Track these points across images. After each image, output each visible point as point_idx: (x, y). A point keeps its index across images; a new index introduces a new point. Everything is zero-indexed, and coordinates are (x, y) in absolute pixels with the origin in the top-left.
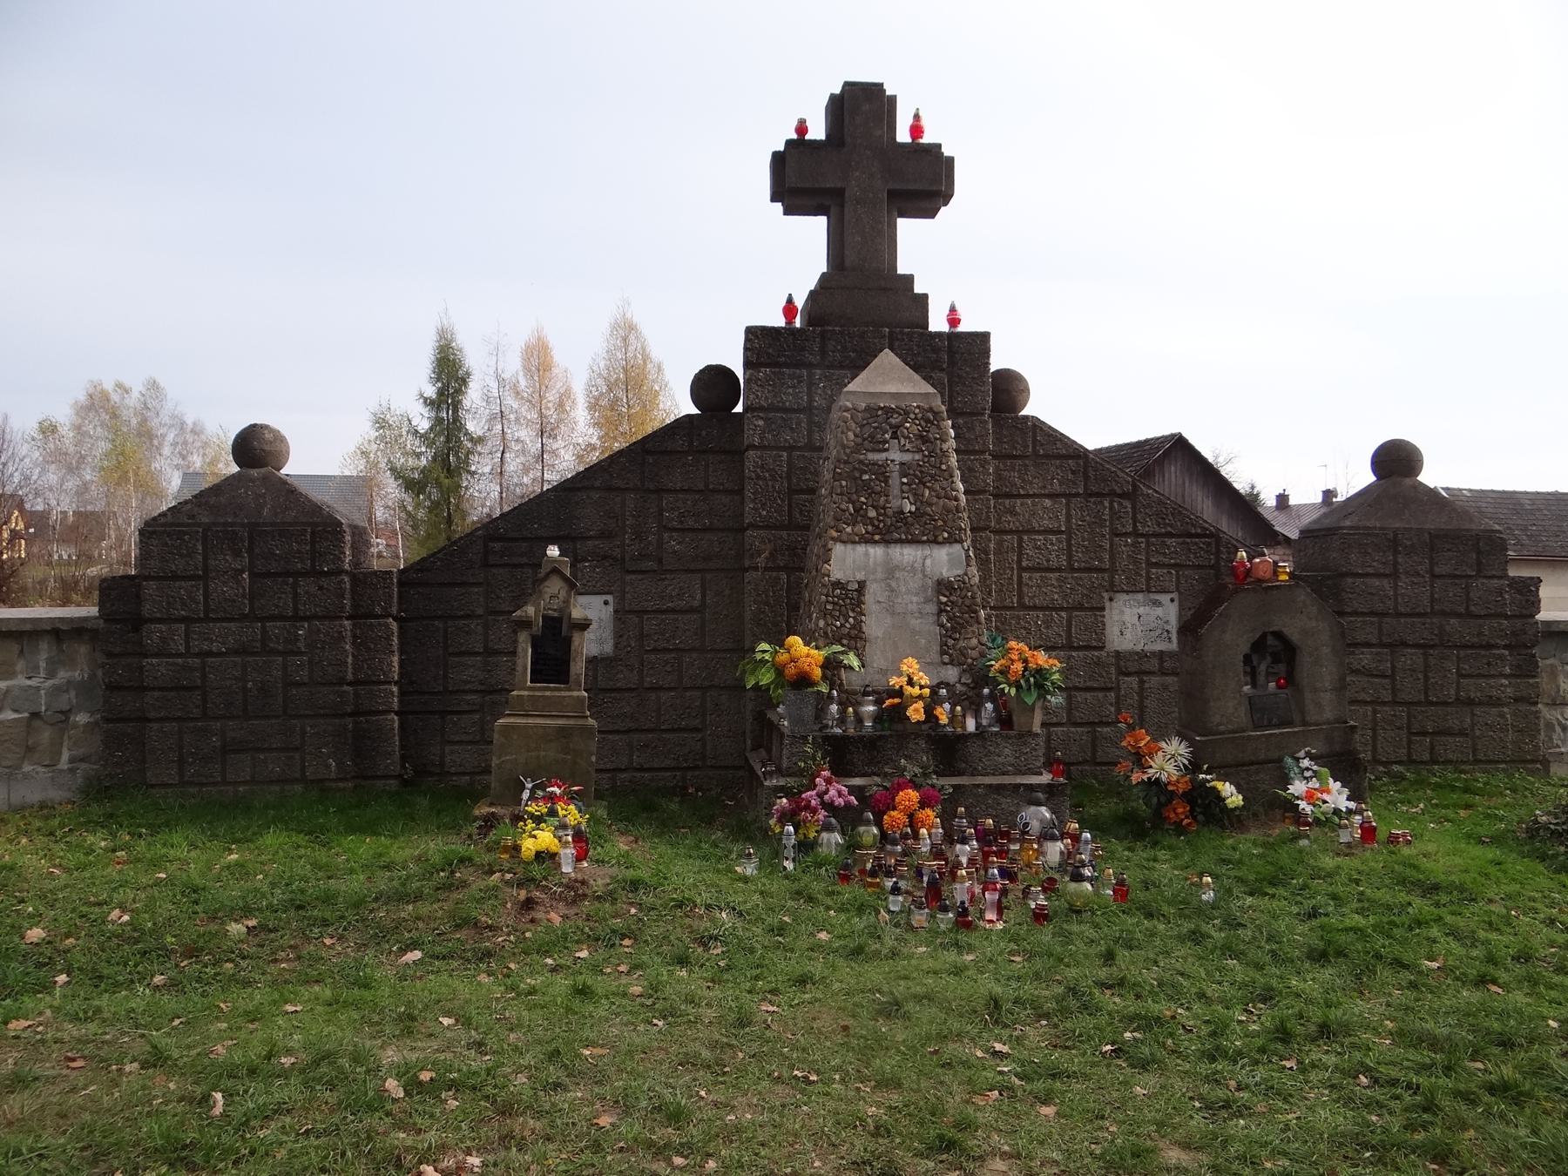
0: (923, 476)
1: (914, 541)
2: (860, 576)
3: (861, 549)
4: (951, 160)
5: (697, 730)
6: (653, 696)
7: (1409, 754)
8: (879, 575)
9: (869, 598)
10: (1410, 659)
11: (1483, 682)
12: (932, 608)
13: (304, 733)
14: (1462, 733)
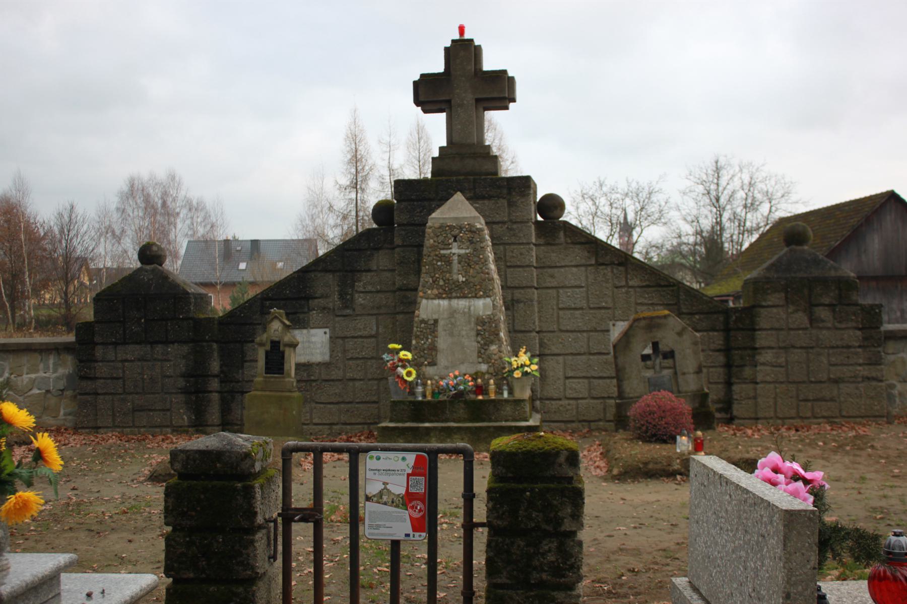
0: (472, 261)
2: (435, 317)
3: (436, 302)
4: (513, 78)
6: (351, 384)
8: (445, 316)
9: (440, 328)
11: (845, 369)
12: (473, 333)
13: (171, 401)
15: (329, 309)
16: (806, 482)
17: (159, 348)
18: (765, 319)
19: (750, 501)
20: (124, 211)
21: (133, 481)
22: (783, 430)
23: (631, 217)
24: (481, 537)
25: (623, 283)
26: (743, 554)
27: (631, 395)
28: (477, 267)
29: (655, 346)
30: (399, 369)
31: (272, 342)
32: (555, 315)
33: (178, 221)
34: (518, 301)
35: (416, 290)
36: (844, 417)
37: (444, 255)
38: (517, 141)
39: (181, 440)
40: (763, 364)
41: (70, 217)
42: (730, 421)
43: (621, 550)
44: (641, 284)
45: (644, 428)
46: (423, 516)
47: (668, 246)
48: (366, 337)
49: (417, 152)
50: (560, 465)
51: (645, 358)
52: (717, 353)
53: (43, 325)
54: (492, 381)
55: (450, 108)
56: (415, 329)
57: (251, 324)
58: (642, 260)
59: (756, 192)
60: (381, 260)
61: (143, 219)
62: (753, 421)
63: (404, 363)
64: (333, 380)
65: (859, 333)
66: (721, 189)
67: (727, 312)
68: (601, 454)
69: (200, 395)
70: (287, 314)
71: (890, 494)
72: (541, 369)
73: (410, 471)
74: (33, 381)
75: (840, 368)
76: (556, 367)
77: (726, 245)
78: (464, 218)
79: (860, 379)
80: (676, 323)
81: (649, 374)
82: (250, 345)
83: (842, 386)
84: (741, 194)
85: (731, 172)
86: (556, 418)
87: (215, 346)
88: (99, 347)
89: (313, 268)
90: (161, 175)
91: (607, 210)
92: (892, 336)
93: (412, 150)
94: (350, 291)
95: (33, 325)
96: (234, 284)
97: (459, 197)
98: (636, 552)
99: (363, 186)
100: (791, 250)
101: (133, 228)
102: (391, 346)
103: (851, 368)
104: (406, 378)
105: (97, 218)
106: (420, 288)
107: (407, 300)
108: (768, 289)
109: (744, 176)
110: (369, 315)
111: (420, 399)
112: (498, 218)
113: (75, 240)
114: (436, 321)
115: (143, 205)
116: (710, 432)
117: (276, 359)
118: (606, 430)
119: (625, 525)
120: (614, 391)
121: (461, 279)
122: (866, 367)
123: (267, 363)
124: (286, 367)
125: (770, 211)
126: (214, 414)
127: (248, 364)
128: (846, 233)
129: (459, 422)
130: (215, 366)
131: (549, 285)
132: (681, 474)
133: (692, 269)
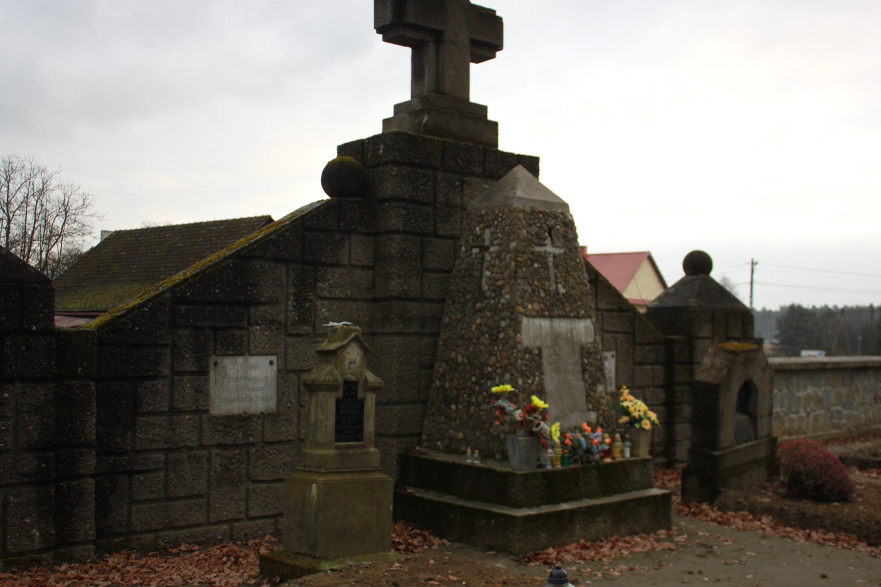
1: (566, 316)
3: (537, 321)
8: (548, 343)
15: (280, 323)
31: (347, 383)
44: (610, 307)
60: (356, 250)
64: (280, 442)
82: (149, 384)
87: (93, 386)
94: (311, 296)
123: (338, 422)
130: (90, 427)
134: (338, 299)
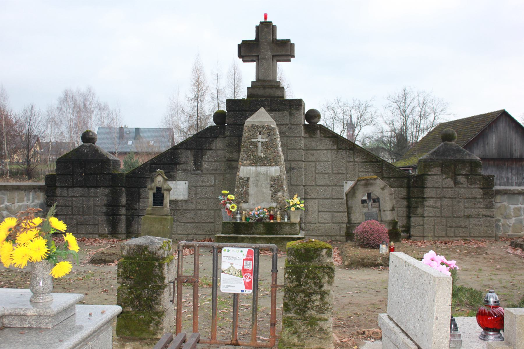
0: (268, 146)
2: (248, 176)
3: (249, 168)
4: (293, 44)
5: (212, 223)
6: (199, 212)
7: (446, 234)
8: (254, 176)
10: (446, 202)
11: (473, 210)
12: (269, 186)
14: (465, 227)
15: (188, 170)
16: (448, 266)
17: (93, 190)
18: (430, 181)
19: (419, 274)
20: (61, 109)
21: (81, 263)
22: (438, 243)
23: (354, 120)
24: (280, 295)
25: (352, 160)
26: (415, 299)
27: (355, 222)
28: (272, 149)
29: (369, 195)
30: (228, 204)
32: (314, 176)
33: (93, 116)
34: (294, 169)
35: (237, 161)
36: (472, 237)
37: (254, 142)
38: (294, 79)
39: (104, 241)
40: (428, 206)
41: (31, 112)
42: (409, 238)
43: (350, 303)
45: (362, 240)
46: (251, 281)
47: (375, 137)
48: (208, 186)
49: (233, 80)
50: (323, 256)
51: (363, 202)
52: (403, 200)
53: (14, 175)
54: (278, 213)
55: (258, 60)
56: (237, 183)
57: (144, 178)
58: (361, 146)
59: (427, 108)
61: (73, 114)
62: (422, 238)
63: (230, 201)
64: (189, 210)
65: (481, 191)
66: (406, 105)
67: (409, 177)
68: (338, 254)
69: (115, 217)
70: (165, 173)
71: (494, 278)
72: (305, 207)
73: (245, 258)
74: (20, 207)
75: (470, 209)
76: (314, 205)
77: (409, 138)
78: (265, 122)
79: (481, 216)
80: (380, 183)
81: (365, 210)
82: (143, 189)
83: (471, 219)
84: (418, 109)
85: (413, 96)
86: (313, 234)
87: (124, 189)
88: (59, 189)
89: (180, 147)
90: (84, 89)
91: (341, 116)
92: (499, 192)
93: (230, 79)
95: (9, 174)
96: (125, 153)
97: (262, 110)
98: (359, 305)
99: (202, 99)
100: (445, 144)
101: (66, 119)
102: (223, 192)
103: (476, 210)
104: (231, 209)
105: (47, 114)
106: (240, 160)
107: (232, 166)
108: (432, 165)
109: (420, 99)
110: (210, 174)
111: (239, 221)
112: (284, 122)
113: (33, 126)
114: (248, 179)
115: (72, 106)
116: (398, 243)
117: (159, 198)
118: (340, 241)
119: (352, 291)
120: (346, 220)
121: (263, 155)
122: (485, 210)
123: (154, 200)
124: (165, 202)
125: (434, 119)
126: (122, 227)
127: (142, 200)
128: (477, 133)
129: (260, 234)
130: (124, 200)
131: (310, 159)
132: (382, 265)
133: (389, 151)
134: (211, 161)
